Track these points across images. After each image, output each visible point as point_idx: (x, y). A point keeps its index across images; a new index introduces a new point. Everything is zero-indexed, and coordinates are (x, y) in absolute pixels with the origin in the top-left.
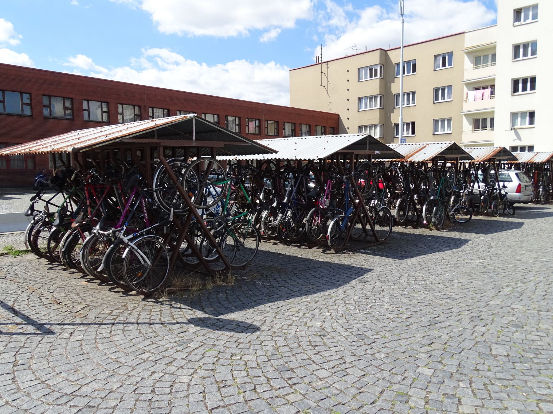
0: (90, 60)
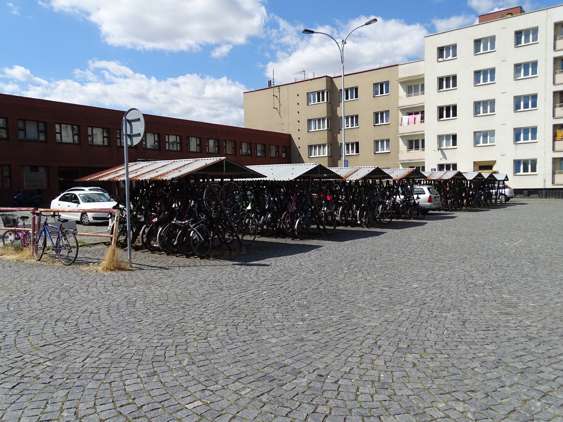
0: (28, 72)
